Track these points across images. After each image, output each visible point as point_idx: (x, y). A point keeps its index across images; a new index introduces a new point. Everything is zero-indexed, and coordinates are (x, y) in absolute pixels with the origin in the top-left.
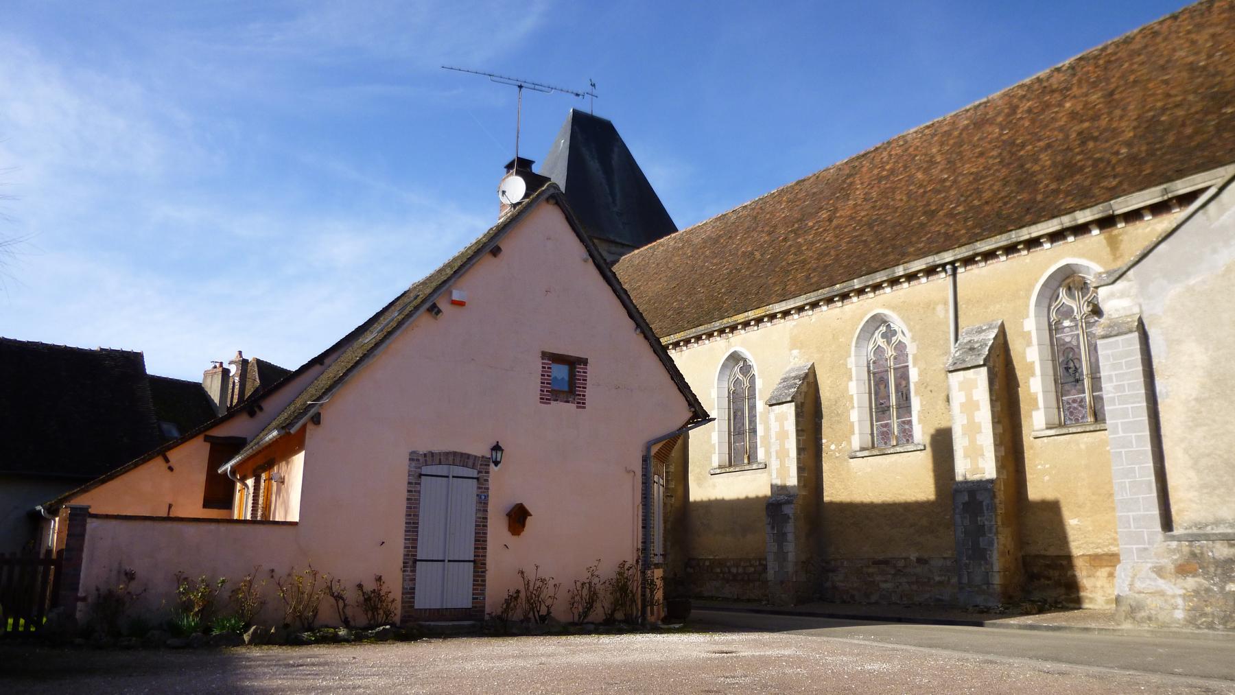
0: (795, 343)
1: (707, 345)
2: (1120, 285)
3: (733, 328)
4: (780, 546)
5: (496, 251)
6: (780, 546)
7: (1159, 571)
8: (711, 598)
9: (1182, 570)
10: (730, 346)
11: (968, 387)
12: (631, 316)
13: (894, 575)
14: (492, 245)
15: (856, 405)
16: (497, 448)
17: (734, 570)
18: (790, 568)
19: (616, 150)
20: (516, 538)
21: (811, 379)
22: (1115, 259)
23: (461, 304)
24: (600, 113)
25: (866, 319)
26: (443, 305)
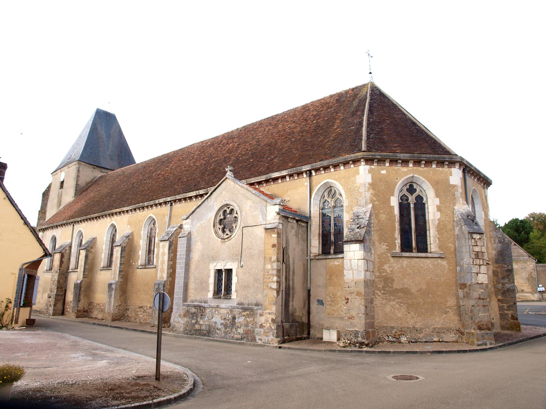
0: (129, 223)
2: (188, 220)
3: (112, 214)
4: (110, 299)
6: (110, 299)
7: (180, 316)
8: (96, 318)
9: (185, 316)
10: (111, 221)
11: (164, 247)
12: (22, 218)
18: (112, 308)
21: (130, 237)
22: (329, 189)
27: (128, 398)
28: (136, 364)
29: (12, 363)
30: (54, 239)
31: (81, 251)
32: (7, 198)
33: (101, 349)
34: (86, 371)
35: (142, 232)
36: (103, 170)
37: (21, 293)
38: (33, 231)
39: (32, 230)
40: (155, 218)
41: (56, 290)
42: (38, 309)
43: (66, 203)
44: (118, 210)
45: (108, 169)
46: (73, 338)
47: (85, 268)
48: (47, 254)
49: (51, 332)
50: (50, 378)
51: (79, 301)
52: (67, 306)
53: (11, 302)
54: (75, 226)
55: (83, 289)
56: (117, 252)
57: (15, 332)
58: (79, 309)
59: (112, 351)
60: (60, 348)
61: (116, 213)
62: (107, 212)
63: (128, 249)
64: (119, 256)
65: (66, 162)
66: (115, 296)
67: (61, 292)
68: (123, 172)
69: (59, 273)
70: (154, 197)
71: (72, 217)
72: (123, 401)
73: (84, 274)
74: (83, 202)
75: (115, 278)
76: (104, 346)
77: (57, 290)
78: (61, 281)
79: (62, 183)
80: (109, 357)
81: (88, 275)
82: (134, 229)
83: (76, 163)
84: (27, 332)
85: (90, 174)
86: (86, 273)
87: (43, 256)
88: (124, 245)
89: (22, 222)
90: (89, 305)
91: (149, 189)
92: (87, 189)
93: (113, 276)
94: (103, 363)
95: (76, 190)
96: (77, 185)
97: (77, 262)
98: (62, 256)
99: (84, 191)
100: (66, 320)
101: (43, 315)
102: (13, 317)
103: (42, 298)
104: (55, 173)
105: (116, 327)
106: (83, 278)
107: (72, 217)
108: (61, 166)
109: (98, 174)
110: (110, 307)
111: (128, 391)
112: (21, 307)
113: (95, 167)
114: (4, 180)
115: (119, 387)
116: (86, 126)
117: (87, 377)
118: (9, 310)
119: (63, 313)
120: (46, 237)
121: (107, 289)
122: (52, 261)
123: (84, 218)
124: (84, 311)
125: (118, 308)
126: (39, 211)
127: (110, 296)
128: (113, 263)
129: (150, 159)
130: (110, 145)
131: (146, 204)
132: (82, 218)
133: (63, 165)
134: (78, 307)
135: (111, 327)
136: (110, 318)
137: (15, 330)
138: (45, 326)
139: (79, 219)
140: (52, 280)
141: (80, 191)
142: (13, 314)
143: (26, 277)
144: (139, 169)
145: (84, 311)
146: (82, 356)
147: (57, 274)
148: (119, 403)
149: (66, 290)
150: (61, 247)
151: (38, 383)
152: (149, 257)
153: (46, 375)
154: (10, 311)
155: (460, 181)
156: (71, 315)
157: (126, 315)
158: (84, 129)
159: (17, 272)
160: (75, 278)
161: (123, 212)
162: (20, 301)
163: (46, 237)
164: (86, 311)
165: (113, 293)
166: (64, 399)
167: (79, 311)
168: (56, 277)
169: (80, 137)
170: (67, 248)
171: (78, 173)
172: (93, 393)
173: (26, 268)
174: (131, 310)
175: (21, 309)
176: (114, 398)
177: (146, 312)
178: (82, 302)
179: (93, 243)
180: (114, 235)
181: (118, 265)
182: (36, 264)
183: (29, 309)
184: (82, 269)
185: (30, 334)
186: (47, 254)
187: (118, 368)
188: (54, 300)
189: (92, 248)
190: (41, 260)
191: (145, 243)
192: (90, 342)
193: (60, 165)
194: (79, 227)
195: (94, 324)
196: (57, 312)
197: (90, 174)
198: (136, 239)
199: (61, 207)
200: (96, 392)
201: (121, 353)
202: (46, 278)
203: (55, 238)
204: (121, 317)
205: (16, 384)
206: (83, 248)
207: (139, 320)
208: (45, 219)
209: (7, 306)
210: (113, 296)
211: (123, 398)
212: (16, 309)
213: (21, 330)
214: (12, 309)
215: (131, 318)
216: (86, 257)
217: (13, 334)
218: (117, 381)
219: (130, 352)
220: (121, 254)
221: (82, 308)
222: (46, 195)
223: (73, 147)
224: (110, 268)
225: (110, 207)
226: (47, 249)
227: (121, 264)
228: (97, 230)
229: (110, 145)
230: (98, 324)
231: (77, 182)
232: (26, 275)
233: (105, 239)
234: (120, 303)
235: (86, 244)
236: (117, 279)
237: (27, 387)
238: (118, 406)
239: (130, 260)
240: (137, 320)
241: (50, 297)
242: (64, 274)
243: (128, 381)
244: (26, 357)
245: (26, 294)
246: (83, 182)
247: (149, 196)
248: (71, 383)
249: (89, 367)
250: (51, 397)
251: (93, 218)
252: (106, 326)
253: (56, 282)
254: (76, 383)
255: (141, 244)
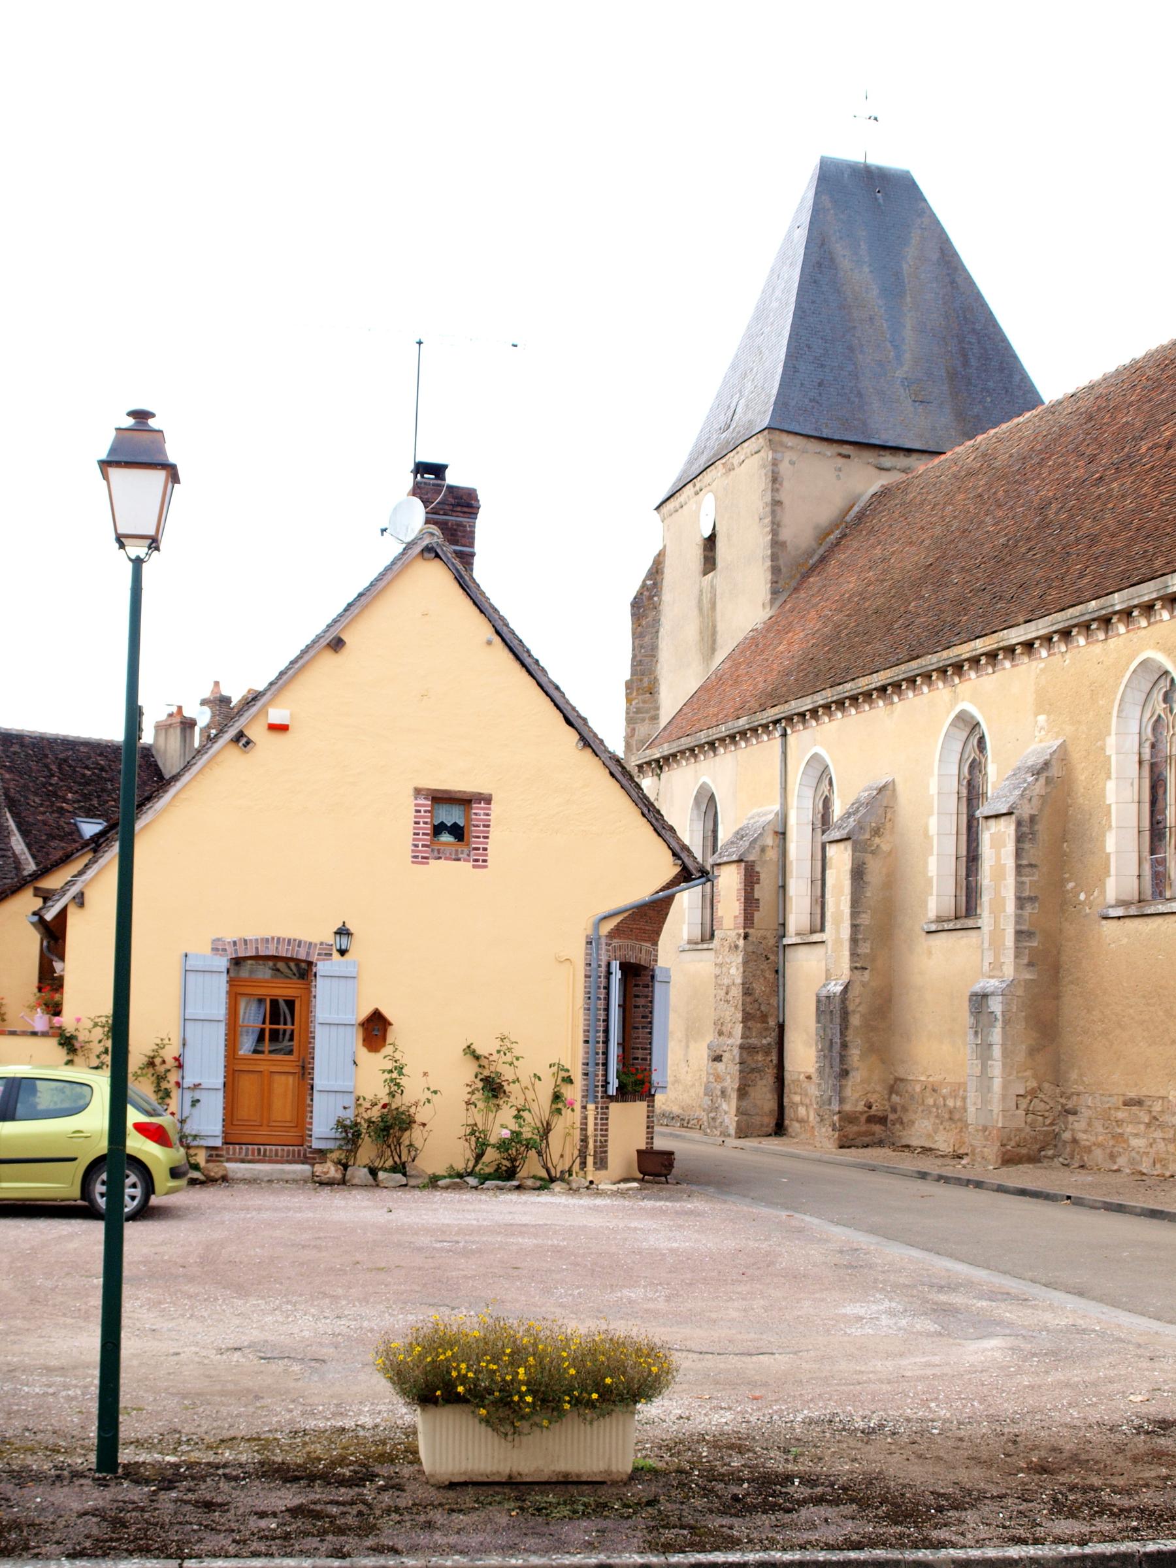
0: (1044, 704)
1: (911, 703)
3: (958, 667)
4: (984, 1067)
5: (337, 644)
6: (984, 1067)
8: (926, 1150)
10: (955, 699)
13: (1148, 1125)
14: (330, 636)
15: (1114, 824)
16: (343, 932)
17: (950, 1103)
18: (996, 1107)
19: (915, 237)
20: (372, 1055)
21: (1054, 771)
23: (282, 728)
24: (884, 157)
25: (1132, 668)
26: (256, 732)
27: (1124, 1512)
28: (1145, 1364)
29: (622, 1328)
30: (708, 804)
31: (832, 850)
32: (497, 640)
33: (968, 1286)
34: (919, 1379)
35: (1111, 741)
36: (888, 460)
37: (606, 1042)
38: (622, 775)
39: (617, 770)
40: (1169, 667)
41: (738, 1029)
42: (676, 1110)
43: (740, 637)
44: (981, 645)
45: (909, 451)
46: (841, 1234)
47: (854, 927)
48: (689, 873)
49: (744, 1207)
50: (771, 1397)
51: (845, 1073)
52: (793, 1097)
53: (569, 1080)
54: (792, 738)
55: (855, 1020)
56: (998, 845)
57: (599, 1201)
58: (848, 1107)
59: (1023, 1301)
60: (795, 1277)
61: (975, 661)
62: (931, 661)
63: (1051, 829)
64: (1010, 863)
65: (714, 445)
66: (1006, 1054)
67: (761, 1035)
68: (986, 456)
69: (746, 953)
70: (1158, 563)
71: (774, 697)
72: (1103, 1525)
73: (854, 955)
74: (813, 624)
75: (996, 966)
76: (980, 1275)
77: (746, 1028)
78: (759, 988)
79: (711, 542)
80: (1010, 1324)
81: (873, 958)
82: (1069, 729)
83: (761, 441)
84: (648, 1204)
85: (832, 486)
86: (865, 948)
87: (674, 883)
88: (1026, 811)
89: (572, 736)
90: (892, 1090)
91: (1124, 525)
92: (823, 560)
93: (989, 958)
94: (987, 1350)
95: (776, 570)
96: (777, 544)
97: (821, 902)
98: (751, 878)
99: (812, 570)
100: (798, 1157)
101: (696, 1135)
102: (584, 1140)
103: (691, 1055)
104: (671, 505)
105: (1022, 1192)
106: (854, 969)
107: (774, 697)
108: (696, 469)
109: (864, 480)
110: (985, 1102)
111: (1120, 1482)
112: (612, 1098)
113: (846, 449)
114: (477, 562)
115: (1075, 1458)
116: (782, 256)
117: (925, 1403)
118: (567, 1112)
119: (779, 1129)
120: (674, 791)
121: (965, 1017)
122: (710, 902)
123: (829, 695)
124: (871, 1120)
125: (1024, 1103)
126: (629, 685)
127: (984, 1050)
128: (986, 899)
129: (1111, 368)
130: (908, 333)
131: (1118, 601)
132: (820, 699)
133: (702, 462)
134: (842, 1101)
135: (1001, 1189)
136: (992, 1152)
137: (599, 1193)
138: (714, 1181)
139: (806, 704)
140: (718, 986)
141: (793, 573)
142: (584, 1129)
143: (617, 975)
144: (1064, 431)
145: (871, 1120)
146: (891, 1313)
147: (738, 958)
148: (1085, 1529)
149: (781, 1027)
150: (740, 835)
151: (729, 1416)
152: (1156, 863)
153: (753, 1384)
154: (569, 1119)
155: (239, 698)
156: (811, 1130)
157: (1067, 1136)
158: (775, 273)
159: (578, 952)
160: (817, 971)
161: (1010, 650)
162: (606, 1075)
163: (674, 791)
164: (882, 1120)
165: (996, 1035)
166: (845, 1489)
167: (848, 1118)
168: (735, 972)
169: (761, 314)
170: (769, 840)
171: (775, 490)
172: (963, 1475)
173: (612, 935)
174: (1085, 1113)
175: (613, 1106)
176: (1059, 1508)
177: (1162, 1126)
178: (856, 1077)
179: (879, 807)
180: (976, 767)
181: (1010, 907)
182: (648, 917)
183: (640, 1107)
184: (846, 932)
185: (663, 1212)
186: (689, 873)
187: (1059, 1376)
188: (735, 1069)
189: (877, 832)
190: (669, 900)
191: (1131, 793)
192: (915, 1253)
193: (691, 462)
194: (808, 742)
195: (923, 1176)
196: (757, 1120)
197: (832, 486)
198: (1082, 776)
199: (720, 656)
200: (977, 1472)
201: (1065, 1311)
202: (695, 977)
203: (712, 798)
204: (1040, 1148)
205: (647, 1410)
206: (836, 835)
207: (1132, 1161)
208: (655, 718)
209: (557, 1097)
210: (997, 1051)
211: (1103, 1510)
212: (591, 1107)
213: (623, 1194)
214: (578, 1107)
215: (1089, 1150)
216: (858, 874)
217: (596, 1209)
218: (1065, 1432)
219: (1106, 1309)
220: (1018, 854)
221: (861, 1107)
222: (645, 606)
223: (734, 367)
224: (970, 923)
225: (940, 638)
226: (686, 848)
227: (1021, 901)
228: (894, 748)
229: (908, 333)
230: (940, 1178)
231: (775, 527)
232: (615, 966)
233: (933, 789)
234: (1033, 1084)
235: (849, 815)
236: (1009, 971)
237: (688, 1427)
238: (1083, 1543)
239: (1063, 882)
240: (1122, 1161)
241: (718, 1058)
242: (766, 958)
243: (1117, 1438)
244: (662, 1305)
245: (624, 1044)
246: (800, 530)
247: (1130, 560)
248: (860, 1424)
249: (929, 1365)
250: (788, 1478)
251: (868, 695)
252: (979, 1185)
253: (736, 992)
254: (881, 1426)
255: (1111, 797)
